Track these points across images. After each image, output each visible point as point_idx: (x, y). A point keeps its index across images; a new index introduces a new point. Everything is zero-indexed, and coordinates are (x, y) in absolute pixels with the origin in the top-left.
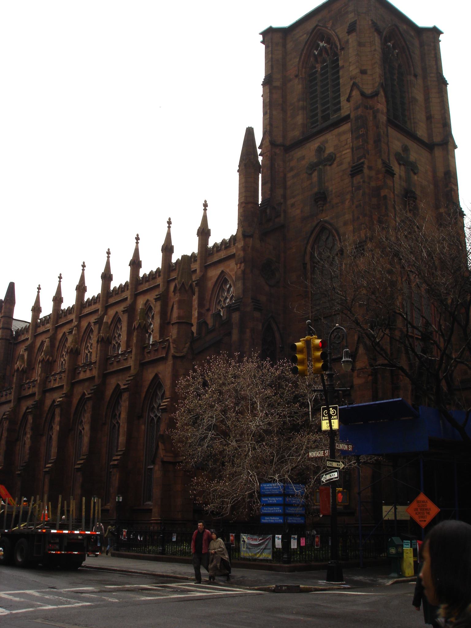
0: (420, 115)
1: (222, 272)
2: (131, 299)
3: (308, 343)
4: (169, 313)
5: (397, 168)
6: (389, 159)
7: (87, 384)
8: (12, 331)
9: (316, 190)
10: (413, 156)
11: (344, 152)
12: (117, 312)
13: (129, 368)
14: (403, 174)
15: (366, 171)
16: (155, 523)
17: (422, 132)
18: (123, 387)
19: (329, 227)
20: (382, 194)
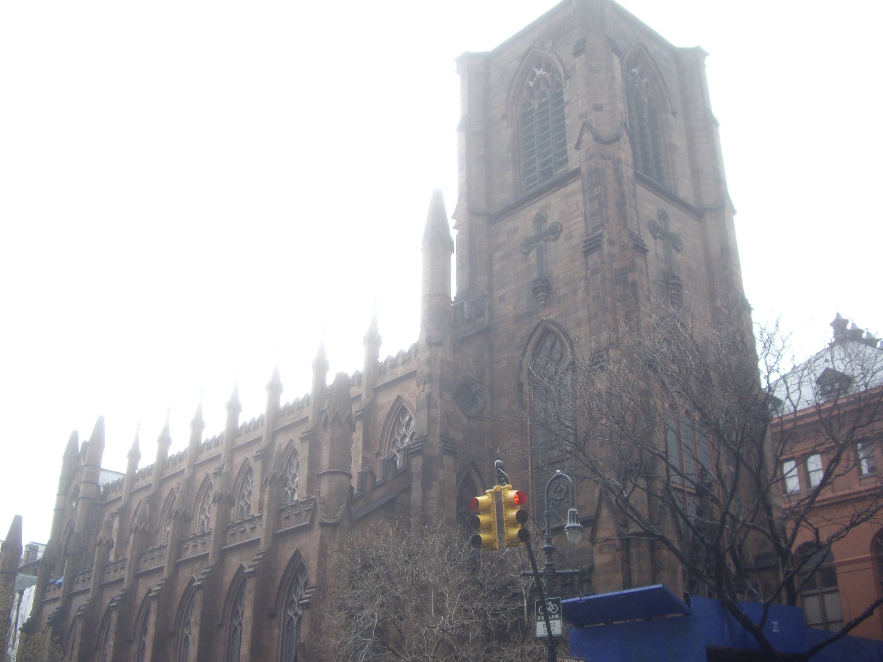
1: (399, 397)
3: (497, 495)
5: (649, 242)
6: (639, 230)
7: (197, 565)
8: (98, 487)
9: (535, 275)
11: (573, 222)
12: (247, 459)
14: (660, 251)
15: (606, 247)
17: (685, 192)
18: (247, 570)
19: (555, 329)
20: (630, 279)
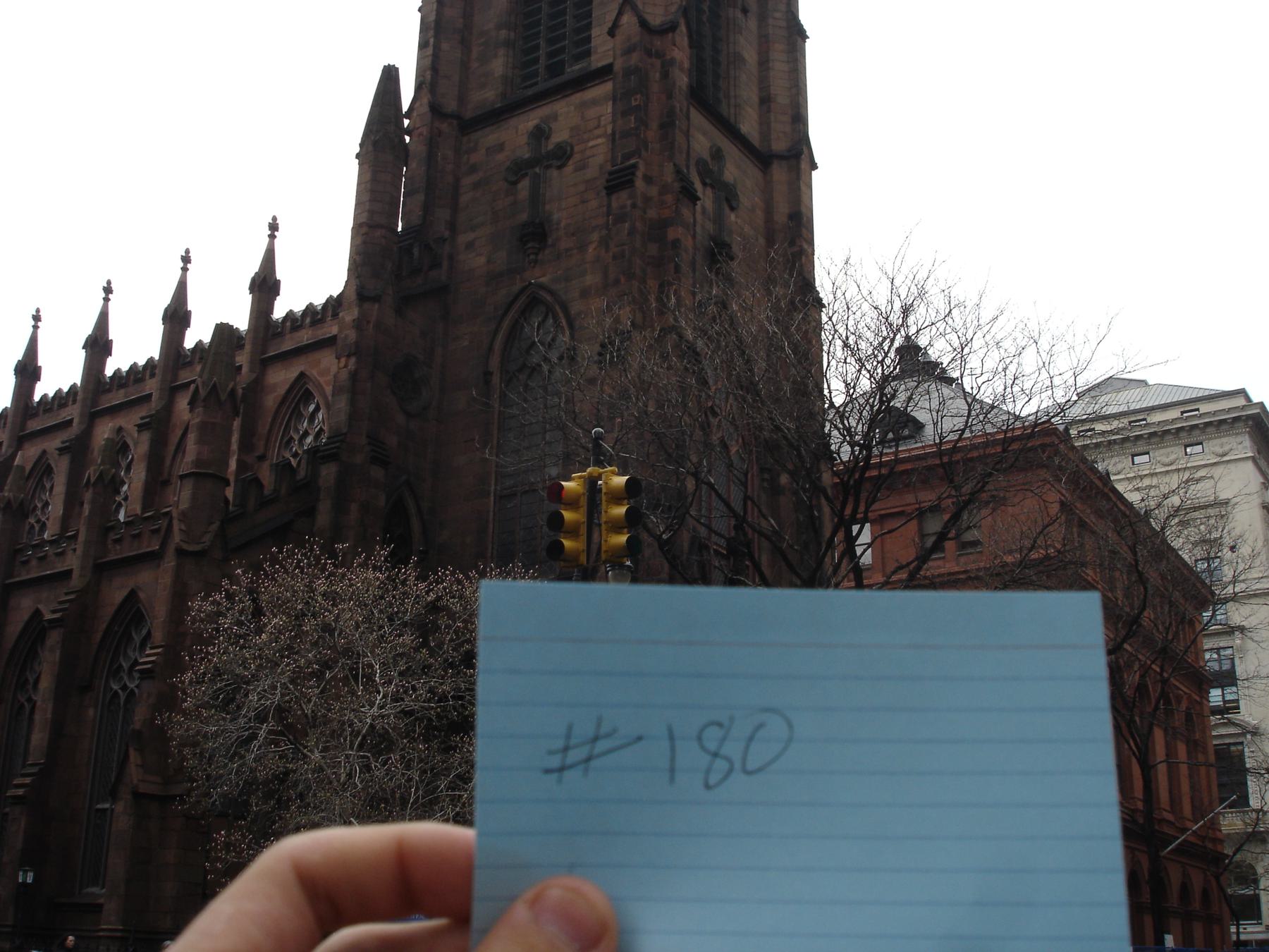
0: (748, 93)
1: (302, 375)
2: (80, 423)
3: (592, 485)
4: (168, 462)
9: (524, 217)
10: (731, 172)
11: (591, 144)
12: (44, 452)
13: (67, 574)
15: (639, 183)
16: (108, 937)
17: (749, 126)
18: (48, 616)
19: (549, 298)
